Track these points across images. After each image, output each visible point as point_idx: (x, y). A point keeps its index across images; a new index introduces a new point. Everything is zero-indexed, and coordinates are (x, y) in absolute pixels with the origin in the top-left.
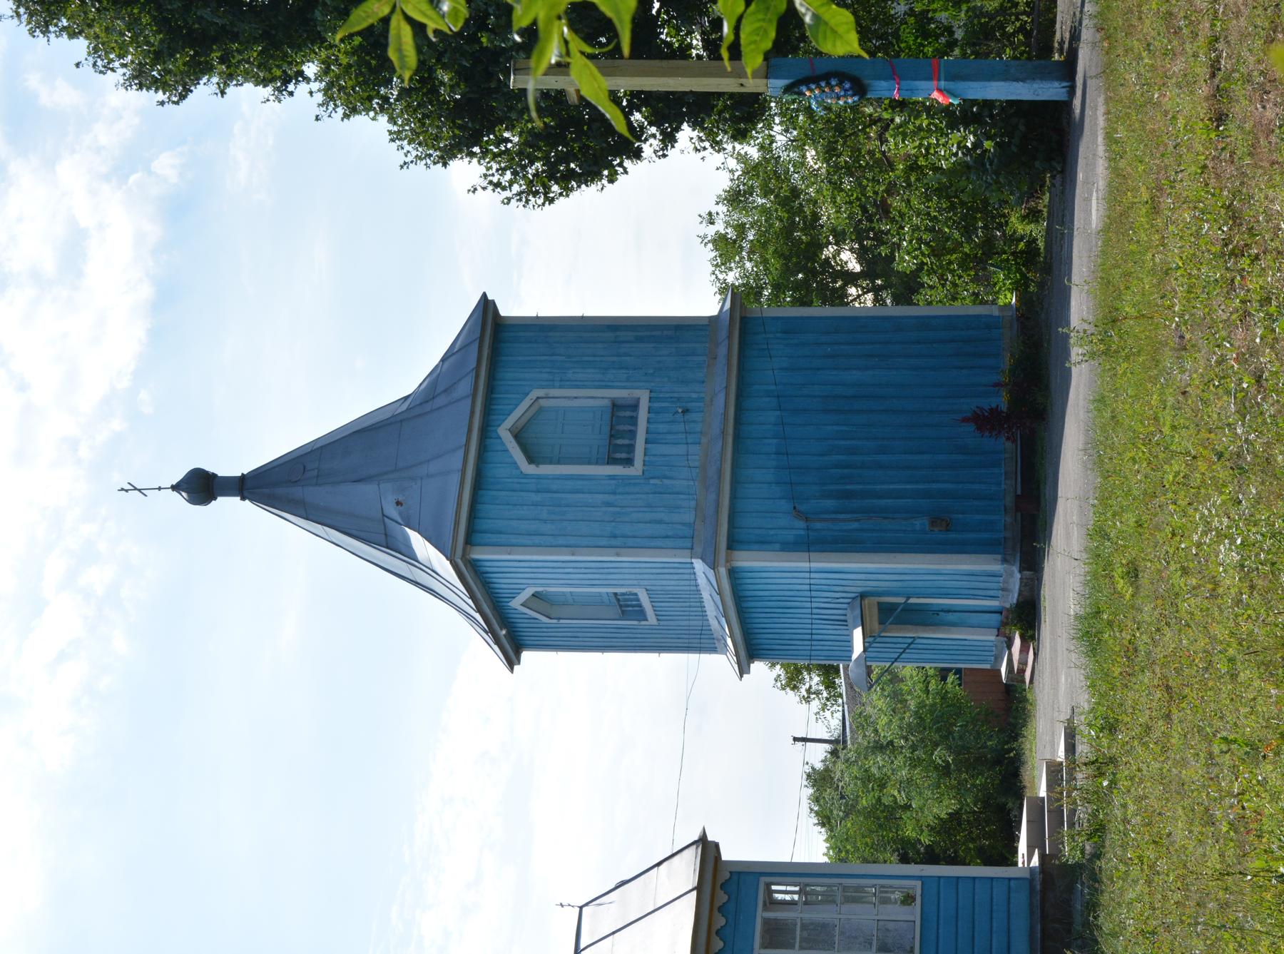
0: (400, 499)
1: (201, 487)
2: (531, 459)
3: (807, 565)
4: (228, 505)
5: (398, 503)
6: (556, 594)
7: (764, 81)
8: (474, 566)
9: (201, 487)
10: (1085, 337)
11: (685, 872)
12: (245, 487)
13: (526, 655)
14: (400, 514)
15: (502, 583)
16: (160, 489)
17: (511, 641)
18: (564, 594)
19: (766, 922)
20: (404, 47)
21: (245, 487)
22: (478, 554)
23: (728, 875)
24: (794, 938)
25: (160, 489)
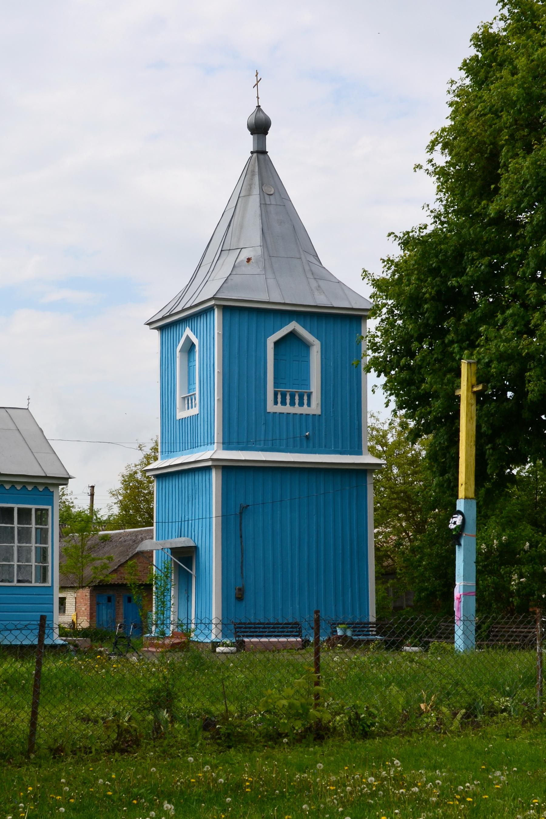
0: (252, 260)
1: (260, 128)
2: (277, 344)
3: (214, 515)
4: (248, 142)
5: (249, 260)
6: (194, 355)
7: (464, 497)
8: (210, 309)
9: (260, 128)
10: (459, 599)
11: (52, 472)
12: (261, 152)
13: (157, 333)
14: (242, 261)
15: (201, 323)
16: (258, 98)
17: (167, 326)
18: (195, 361)
19: (30, 510)
20: (225, 651)
21: (261, 152)
22: (217, 315)
23: (51, 490)
24: (23, 524)
25: (258, 98)
